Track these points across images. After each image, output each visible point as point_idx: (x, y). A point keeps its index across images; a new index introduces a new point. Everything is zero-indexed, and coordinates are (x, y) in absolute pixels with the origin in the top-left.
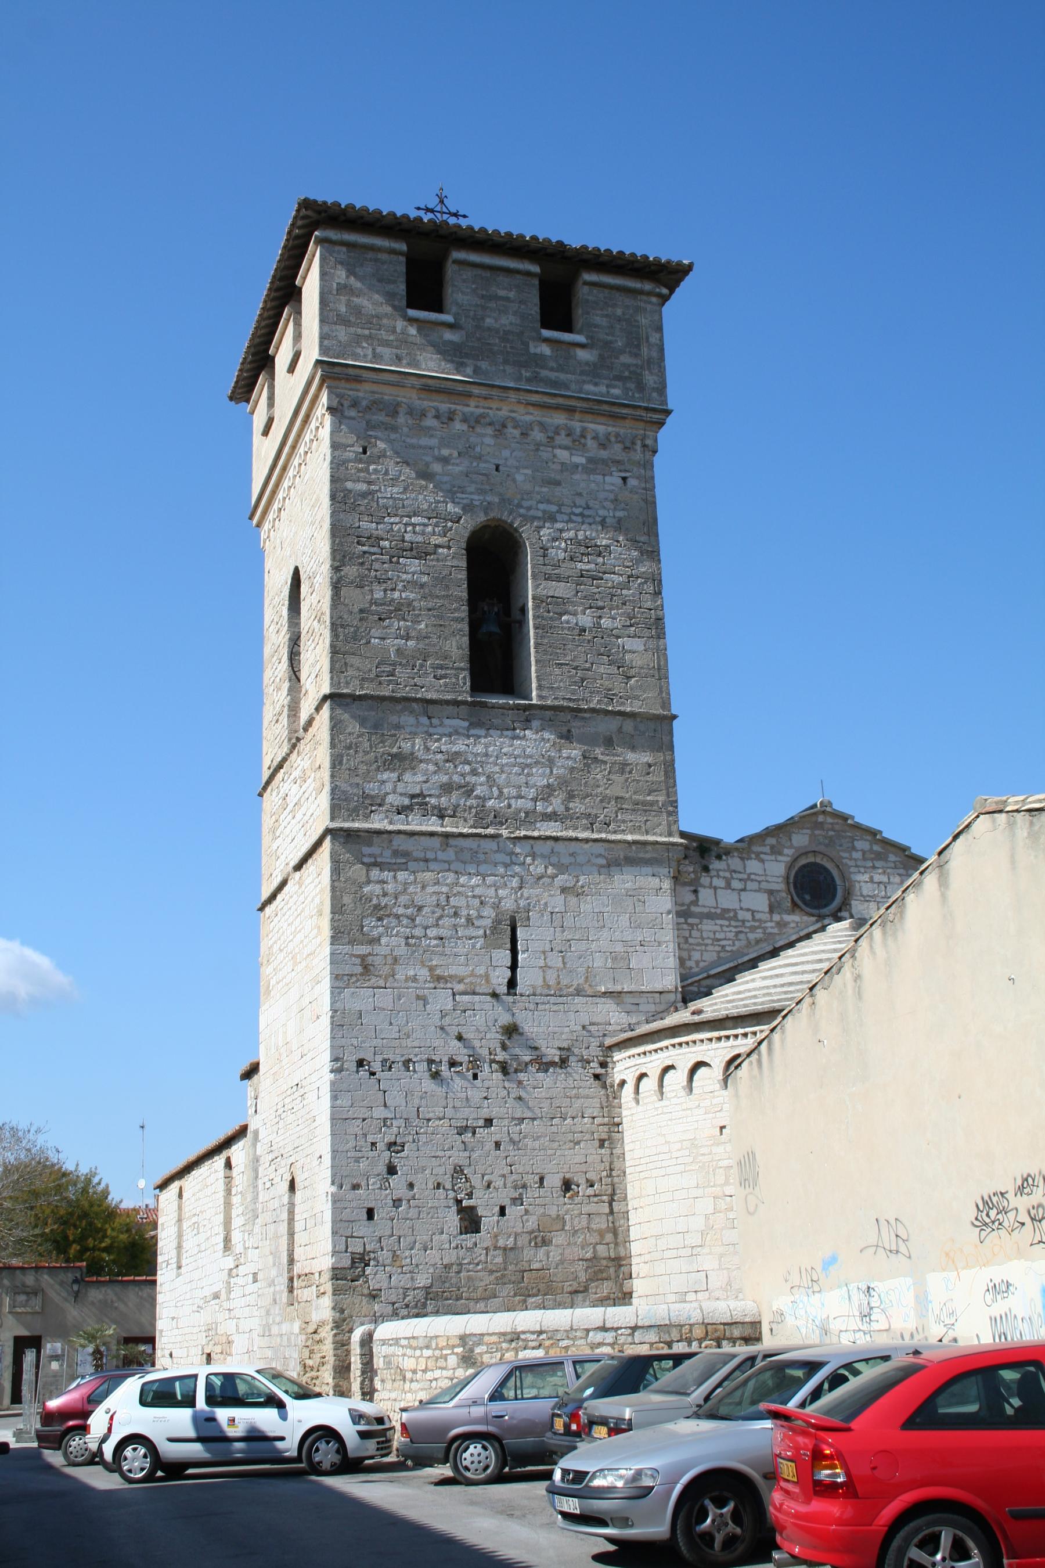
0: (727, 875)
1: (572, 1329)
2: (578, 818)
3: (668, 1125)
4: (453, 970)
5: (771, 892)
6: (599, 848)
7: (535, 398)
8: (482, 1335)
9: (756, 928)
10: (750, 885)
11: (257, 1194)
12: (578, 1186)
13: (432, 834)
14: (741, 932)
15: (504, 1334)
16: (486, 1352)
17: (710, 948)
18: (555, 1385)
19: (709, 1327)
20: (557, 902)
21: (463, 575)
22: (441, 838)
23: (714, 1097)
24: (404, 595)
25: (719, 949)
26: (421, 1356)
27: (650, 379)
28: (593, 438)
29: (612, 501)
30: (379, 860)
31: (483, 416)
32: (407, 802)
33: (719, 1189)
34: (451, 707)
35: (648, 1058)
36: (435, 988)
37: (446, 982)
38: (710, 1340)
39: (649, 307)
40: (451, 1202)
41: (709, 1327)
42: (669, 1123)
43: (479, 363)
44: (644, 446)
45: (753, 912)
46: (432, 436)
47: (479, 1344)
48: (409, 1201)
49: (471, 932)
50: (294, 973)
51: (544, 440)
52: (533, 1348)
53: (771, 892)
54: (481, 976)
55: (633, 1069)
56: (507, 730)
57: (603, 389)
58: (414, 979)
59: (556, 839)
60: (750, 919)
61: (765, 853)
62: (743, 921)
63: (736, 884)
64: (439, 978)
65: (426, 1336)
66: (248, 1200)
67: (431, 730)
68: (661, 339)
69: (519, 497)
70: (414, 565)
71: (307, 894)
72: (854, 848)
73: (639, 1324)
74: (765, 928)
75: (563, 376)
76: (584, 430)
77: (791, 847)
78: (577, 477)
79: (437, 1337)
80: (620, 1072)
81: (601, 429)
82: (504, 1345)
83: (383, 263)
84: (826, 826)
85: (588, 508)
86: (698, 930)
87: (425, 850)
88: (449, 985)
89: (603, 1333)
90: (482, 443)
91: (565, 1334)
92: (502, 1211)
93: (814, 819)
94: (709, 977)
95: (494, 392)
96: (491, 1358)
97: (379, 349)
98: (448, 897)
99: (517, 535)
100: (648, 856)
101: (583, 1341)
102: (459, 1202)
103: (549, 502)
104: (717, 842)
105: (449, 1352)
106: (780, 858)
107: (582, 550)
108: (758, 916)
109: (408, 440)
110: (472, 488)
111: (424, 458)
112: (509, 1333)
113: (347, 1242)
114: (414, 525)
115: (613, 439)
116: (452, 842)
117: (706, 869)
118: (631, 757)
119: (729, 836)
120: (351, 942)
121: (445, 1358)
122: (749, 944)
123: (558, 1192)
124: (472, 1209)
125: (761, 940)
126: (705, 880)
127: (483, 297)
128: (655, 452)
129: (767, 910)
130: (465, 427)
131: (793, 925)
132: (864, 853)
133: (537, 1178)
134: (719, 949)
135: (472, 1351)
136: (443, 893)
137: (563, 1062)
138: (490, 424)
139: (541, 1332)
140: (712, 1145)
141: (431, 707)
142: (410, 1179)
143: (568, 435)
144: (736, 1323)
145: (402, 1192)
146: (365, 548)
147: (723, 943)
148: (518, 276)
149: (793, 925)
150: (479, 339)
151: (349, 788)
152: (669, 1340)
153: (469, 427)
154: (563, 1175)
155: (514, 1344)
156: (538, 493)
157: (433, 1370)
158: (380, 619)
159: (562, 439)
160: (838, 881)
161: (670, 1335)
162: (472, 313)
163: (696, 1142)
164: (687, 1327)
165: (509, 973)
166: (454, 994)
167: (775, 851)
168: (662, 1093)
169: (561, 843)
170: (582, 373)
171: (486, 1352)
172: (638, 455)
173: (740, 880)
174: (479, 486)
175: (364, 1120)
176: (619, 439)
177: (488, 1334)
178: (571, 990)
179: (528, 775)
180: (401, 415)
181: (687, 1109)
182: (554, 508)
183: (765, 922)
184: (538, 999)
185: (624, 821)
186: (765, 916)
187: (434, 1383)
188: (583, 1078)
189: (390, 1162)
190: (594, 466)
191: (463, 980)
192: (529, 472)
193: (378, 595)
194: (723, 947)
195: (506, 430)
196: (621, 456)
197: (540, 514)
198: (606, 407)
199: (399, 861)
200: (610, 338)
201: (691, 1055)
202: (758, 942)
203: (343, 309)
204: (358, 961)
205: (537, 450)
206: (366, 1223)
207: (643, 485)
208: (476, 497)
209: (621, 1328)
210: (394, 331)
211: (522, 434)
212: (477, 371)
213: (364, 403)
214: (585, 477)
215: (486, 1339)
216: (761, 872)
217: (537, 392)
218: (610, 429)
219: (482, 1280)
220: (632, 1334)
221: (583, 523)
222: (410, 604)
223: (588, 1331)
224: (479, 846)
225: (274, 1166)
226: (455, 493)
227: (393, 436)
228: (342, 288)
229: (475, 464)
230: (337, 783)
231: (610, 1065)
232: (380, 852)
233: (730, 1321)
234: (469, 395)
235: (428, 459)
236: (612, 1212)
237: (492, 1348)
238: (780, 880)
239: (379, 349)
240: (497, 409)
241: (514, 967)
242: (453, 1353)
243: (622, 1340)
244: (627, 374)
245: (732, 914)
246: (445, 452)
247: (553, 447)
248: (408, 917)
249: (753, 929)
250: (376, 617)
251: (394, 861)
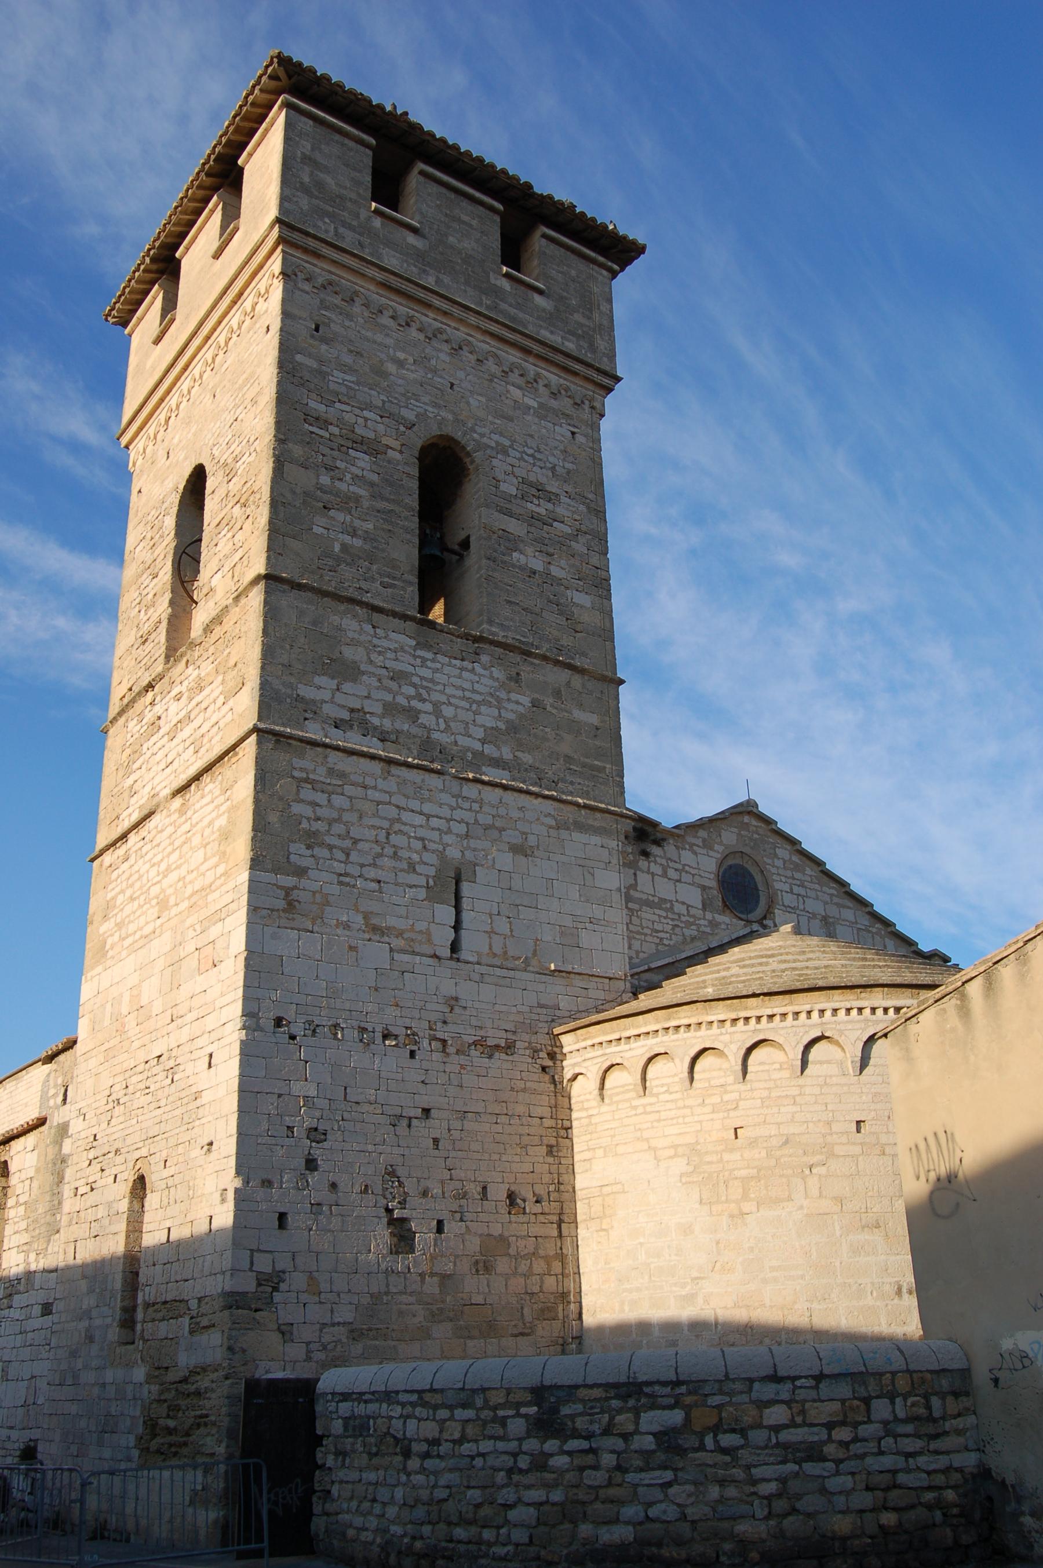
0: (664, 862)
1: (727, 1375)
2: (526, 770)
3: (653, 1127)
4: (391, 921)
5: (704, 888)
6: (549, 806)
7: (494, 328)
8: (577, 1387)
9: (693, 924)
10: (685, 877)
11: (60, 1203)
12: (524, 1201)
13: (373, 757)
14: (677, 926)
15: (616, 1386)
16: (581, 1414)
17: (649, 938)
18: (700, 1465)
19: (915, 1375)
20: (506, 860)
21: (415, 485)
22: (382, 764)
23: (726, 1092)
24: (351, 488)
25: (658, 941)
26: (452, 1418)
27: (601, 344)
28: (545, 386)
29: (561, 451)
30: (311, 776)
31: (441, 331)
32: (345, 715)
33: (733, 1205)
34: (397, 621)
35: (623, 1046)
36: (370, 940)
37: (383, 934)
38: (916, 1395)
39: (600, 278)
40: (382, 1212)
41: (915, 1375)
42: (655, 1124)
43: (441, 276)
44: (593, 408)
45: (688, 906)
46: (387, 335)
47: (568, 1401)
48: (331, 1206)
49: (413, 879)
50: (159, 922)
51: (499, 374)
52: (664, 1408)
53: (704, 888)
54: (421, 932)
55: (600, 1060)
56: (455, 658)
57: (559, 340)
58: (347, 926)
59: (505, 788)
60: (686, 913)
61: (698, 846)
62: (679, 915)
63: (671, 873)
64: (375, 929)
65: (463, 1389)
66: (40, 1211)
67: (375, 641)
68: (611, 311)
69: (473, 421)
70: (364, 461)
71: (194, 822)
72: (776, 855)
73: (826, 1371)
74: (700, 925)
75: (521, 315)
76: (538, 375)
77: (721, 843)
78: (529, 418)
79: (484, 1390)
80: (574, 1065)
81: (554, 379)
82: (615, 1403)
83: (351, 150)
84: (752, 828)
85: (539, 451)
86: (638, 916)
87: (365, 774)
88: (386, 939)
89: (774, 1386)
90: (438, 358)
91: (717, 1386)
92: (440, 1228)
93: (740, 818)
94: (649, 970)
95: (456, 311)
96: (591, 1422)
97: (341, 230)
98: (388, 834)
99: (467, 460)
100: (597, 824)
101: (745, 1398)
102: (389, 1211)
103: (501, 434)
104: (655, 825)
105: (511, 1412)
106: (711, 853)
107: (534, 491)
108: (693, 911)
109: (363, 332)
110: (426, 399)
111: (379, 354)
112: (624, 1384)
113: (252, 1257)
114: (366, 419)
115: (563, 392)
116: (395, 770)
117: (645, 854)
118: (578, 715)
119: (668, 822)
120: (276, 871)
121: (503, 1422)
122: (685, 941)
123: (503, 1209)
124: (403, 1220)
125: (695, 937)
126: (643, 863)
127: (446, 215)
128: (602, 416)
129: (700, 907)
130: (421, 336)
131: (723, 926)
132: (785, 862)
133: (479, 1189)
134: (658, 941)
135: (555, 1410)
136: (382, 829)
137: (509, 1048)
138: (446, 341)
139: (678, 1383)
140: (723, 1151)
141: (376, 616)
142: (332, 1177)
143: (521, 375)
144: (944, 1370)
145: (323, 1195)
146: (311, 429)
147: (661, 935)
148: (481, 208)
149: (723, 926)
150: (442, 254)
151: (281, 687)
152: (866, 1395)
153: (426, 337)
154: (507, 1186)
155: (631, 1403)
156: (492, 423)
157: (476, 1441)
158: (325, 507)
159: (514, 377)
160: (761, 887)
161: (866, 1388)
162: (436, 227)
163: (699, 1147)
164: (888, 1375)
165: (452, 935)
166: (391, 950)
167: (707, 845)
168: (645, 1088)
169: (509, 793)
170: (539, 318)
171: (581, 1414)
172: (585, 414)
173: (676, 870)
174: (433, 399)
175: (280, 1096)
176: (569, 394)
177: (586, 1386)
178: (517, 962)
179: (475, 713)
180: (357, 304)
181: (685, 1107)
182: (507, 443)
183: (700, 919)
184: (484, 969)
185: (572, 783)
186: (699, 913)
187: (478, 1462)
188: (531, 1069)
189: (309, 1153)
190: (544, 412)
191: (401, 934)
192: (483, 399)
193: (325, 480)
194: (661, 939)
195: (461, 352)
196: (570, 410)
197: (493, 444)
198: (560, 358)
199: (334, 782)
200: (565, 294)
201: (694, 1041)
202: (693, 939)
203: (306, 179)
204: (282, 894)
205: (491, 381)
206: (278, 1232)
207: (591, 445)
208: (430, 409)
209: (800, 1377)
210: (357, 216)
211: (478, 360)
212: (438, 281)
213: (320, 280)
214: (536, 420)
215: (582, 1393)
216: (695, 865)
217: (497, 322)
218: (562, 381)
219: (414, 1316)
220: (816, 1387)
221: (534, 465)
222: (357, 499)
223: (751, 1381)
224: (423, 781)
225: (99, 1166)
226: (409, 399)
227: (347, 323)
228: (307, 159)
229: (429, 376)
230: (269, 679)
231: (559, 1057)
232: (313, 768)
233: (937, 1368)
234: (429, 306)
235: (383, 356)
236: (560, 1236)
237: (592, 1408)
238: (712, 876)
239: (341, 230)
240: (455, 328)
241: (457, 927)
242: (518, 1415)
243: (801, 1394)
244: (580, 332)
245: (668, 905)
246: (401, 355)
247: (507, 383)
248: (343, 850)
249: (688, 924)
250: (321, 505)
251: (328, 781)
